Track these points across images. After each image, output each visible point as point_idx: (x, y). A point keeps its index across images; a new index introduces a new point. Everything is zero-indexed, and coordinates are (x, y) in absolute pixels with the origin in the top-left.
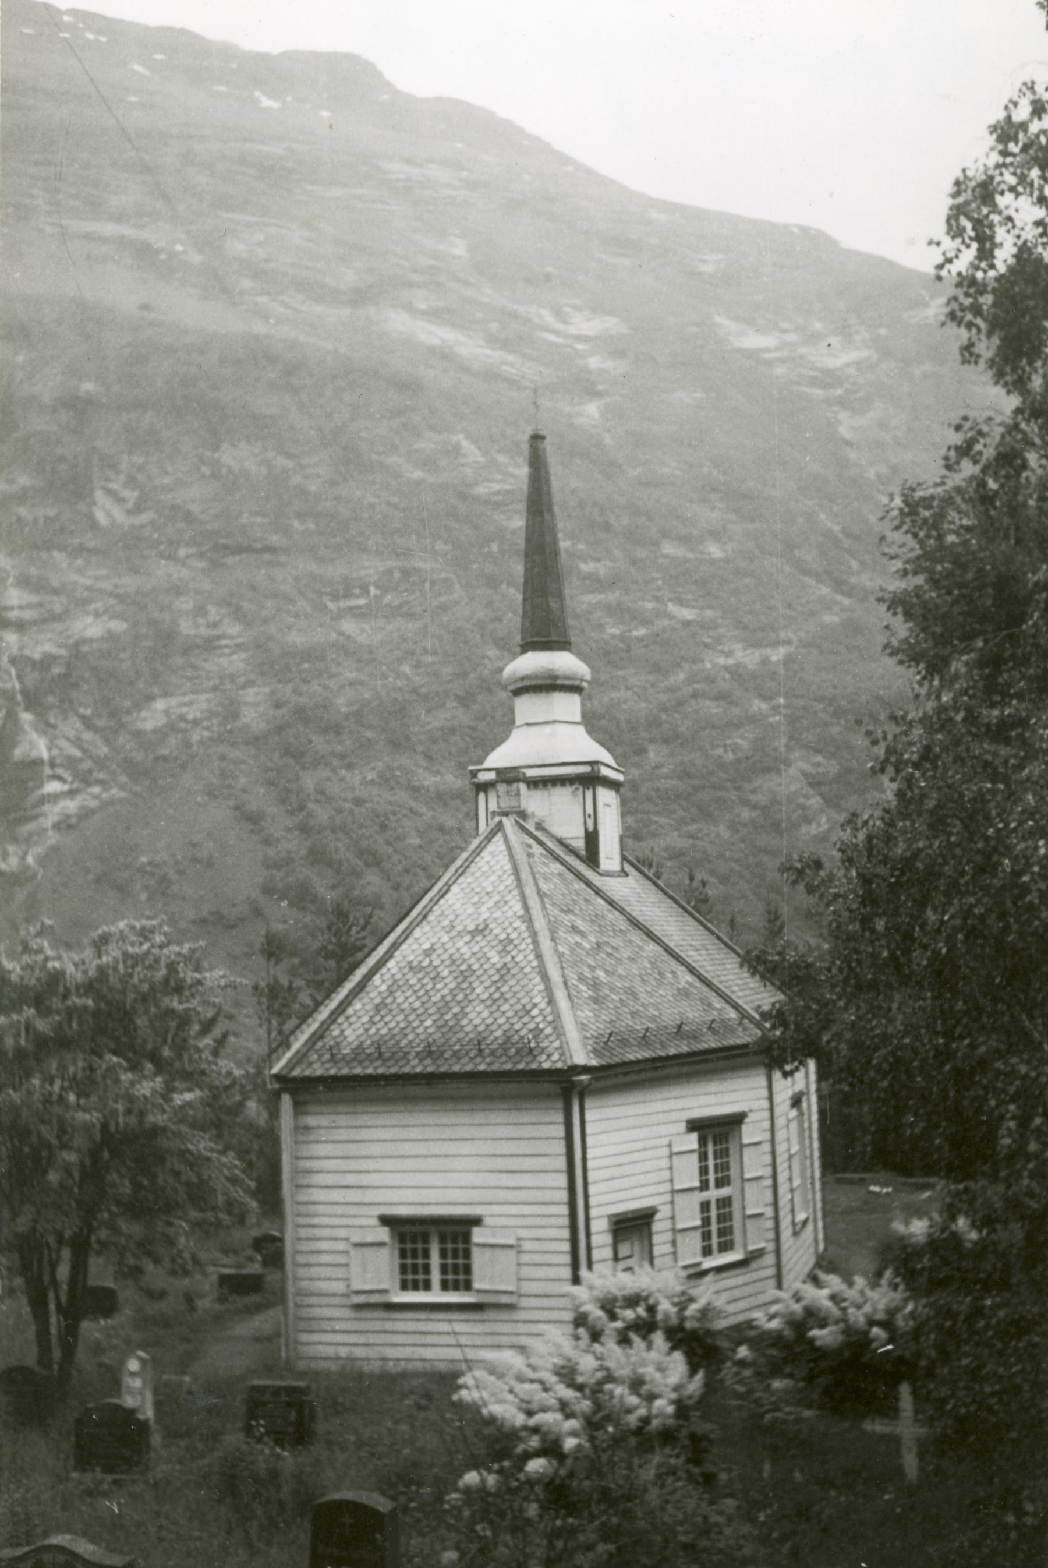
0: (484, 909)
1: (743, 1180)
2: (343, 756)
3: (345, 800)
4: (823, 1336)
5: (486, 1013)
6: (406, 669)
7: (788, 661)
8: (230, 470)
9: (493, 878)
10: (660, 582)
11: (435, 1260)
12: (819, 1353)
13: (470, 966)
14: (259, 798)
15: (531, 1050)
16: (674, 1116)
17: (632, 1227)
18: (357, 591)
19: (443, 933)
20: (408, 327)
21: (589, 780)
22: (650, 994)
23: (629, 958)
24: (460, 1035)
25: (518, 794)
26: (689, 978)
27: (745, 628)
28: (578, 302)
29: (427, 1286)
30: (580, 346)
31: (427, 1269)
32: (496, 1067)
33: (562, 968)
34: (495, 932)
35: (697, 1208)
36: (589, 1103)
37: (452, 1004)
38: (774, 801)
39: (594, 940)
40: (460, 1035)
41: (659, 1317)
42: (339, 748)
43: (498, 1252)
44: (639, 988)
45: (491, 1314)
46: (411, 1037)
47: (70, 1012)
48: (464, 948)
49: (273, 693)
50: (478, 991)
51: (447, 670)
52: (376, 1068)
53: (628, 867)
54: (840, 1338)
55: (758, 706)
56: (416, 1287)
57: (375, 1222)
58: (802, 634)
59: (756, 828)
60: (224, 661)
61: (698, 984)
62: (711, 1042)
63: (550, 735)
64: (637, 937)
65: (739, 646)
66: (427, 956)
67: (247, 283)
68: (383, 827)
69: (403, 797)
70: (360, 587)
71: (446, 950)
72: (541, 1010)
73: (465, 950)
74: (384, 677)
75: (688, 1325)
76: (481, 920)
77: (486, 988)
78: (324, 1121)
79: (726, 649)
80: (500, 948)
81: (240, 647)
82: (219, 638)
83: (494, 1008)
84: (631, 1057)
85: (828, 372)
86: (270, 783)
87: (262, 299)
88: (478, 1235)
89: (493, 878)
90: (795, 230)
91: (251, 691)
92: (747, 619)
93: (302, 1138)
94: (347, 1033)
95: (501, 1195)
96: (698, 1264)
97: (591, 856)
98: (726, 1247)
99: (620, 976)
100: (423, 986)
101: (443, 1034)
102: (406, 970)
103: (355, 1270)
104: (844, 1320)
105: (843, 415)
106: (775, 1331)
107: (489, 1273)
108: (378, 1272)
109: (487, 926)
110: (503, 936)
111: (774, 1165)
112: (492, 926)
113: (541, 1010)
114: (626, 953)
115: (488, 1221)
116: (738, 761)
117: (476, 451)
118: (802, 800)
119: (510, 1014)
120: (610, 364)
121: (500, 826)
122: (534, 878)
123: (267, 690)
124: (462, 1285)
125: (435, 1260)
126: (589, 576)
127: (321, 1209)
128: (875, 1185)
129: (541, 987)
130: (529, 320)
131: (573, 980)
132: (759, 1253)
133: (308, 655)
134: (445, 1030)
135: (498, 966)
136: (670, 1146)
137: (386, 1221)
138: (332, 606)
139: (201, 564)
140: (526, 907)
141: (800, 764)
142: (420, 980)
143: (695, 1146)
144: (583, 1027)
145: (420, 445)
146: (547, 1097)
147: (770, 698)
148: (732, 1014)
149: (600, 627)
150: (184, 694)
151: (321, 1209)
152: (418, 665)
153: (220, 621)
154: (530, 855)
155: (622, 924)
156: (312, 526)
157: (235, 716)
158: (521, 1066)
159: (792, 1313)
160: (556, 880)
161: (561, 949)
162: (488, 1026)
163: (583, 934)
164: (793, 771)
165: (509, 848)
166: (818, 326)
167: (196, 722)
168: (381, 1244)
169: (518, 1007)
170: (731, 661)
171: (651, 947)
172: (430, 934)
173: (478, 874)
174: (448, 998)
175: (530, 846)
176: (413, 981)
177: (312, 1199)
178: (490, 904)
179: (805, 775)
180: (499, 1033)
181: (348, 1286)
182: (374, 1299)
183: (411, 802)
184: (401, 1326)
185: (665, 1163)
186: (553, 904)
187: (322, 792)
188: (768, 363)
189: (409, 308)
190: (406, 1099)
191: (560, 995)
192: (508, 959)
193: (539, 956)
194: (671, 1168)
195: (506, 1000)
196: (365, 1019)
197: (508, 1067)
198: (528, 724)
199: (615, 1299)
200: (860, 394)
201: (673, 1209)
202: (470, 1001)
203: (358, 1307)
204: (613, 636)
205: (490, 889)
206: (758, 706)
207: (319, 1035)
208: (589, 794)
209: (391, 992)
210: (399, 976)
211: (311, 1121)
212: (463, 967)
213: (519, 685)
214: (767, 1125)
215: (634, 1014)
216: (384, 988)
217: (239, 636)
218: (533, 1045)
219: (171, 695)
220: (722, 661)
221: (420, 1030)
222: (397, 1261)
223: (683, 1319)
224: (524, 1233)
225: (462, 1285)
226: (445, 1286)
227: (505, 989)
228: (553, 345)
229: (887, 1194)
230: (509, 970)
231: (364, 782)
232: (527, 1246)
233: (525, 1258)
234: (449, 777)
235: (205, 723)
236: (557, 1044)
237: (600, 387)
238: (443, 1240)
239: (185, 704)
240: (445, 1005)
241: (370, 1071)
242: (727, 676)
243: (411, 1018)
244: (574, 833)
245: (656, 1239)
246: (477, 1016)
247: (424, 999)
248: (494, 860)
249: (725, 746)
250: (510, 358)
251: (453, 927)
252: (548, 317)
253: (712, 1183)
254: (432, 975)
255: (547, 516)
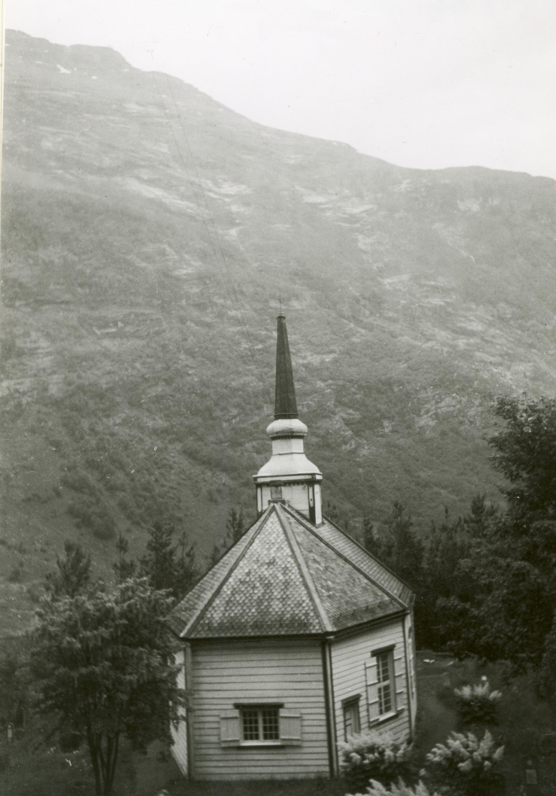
0: (272, 551)
1: (395, 677)
2: (104, 411)
3: (106, 434)
4: (463, 766)
5: (280, 605)
6: (138, 365)
7: (335, 361)
8: (44, 261)
9: (274, 535)
10: (269, 321)
11: (261, 725)
12: (463, 774)
13: (269, 581)
14: (62, 436)
15: (305, 624)
16: (366, 650)
17: (351, 704)
18: (111, 325)
19: (253, 564)
20: (140, 189)
21: (310, 482)
22: (352, 592)
23: (340, 574)
24: (270, 617)
25: (281, 492)
26: (366, 581)
27: (313, 344)
28: (226, 177)
29: (257, 738)
30: (227, 200)
31: (257, 729)
32: (289, 633)
33: (314, 582)
34: (279, 563)
35: (377, 691)
36: (332, 649)
37: (264, 601)
38: (328, 433)
39: (324, 565)
40: (270, 617)
41: (386, 757)
42: (102, 406)
43: (292, 721)
44: (346, 588)
45: (288, 751)
46: (246, 618)
47: (117, 627)
48: (266, 572)
49: (66, 378)
50: (275, 594)
51: (159, 366)
52: (231, 634)
53: (326, 522)
54: (471, 766)
55: (320, 384)
56: (251, 738)
57: (231, 707)
58: (341, 348)
59: (319, 447)
60: (40, 361)
61: (370, 584)
62: (380, 614)
63: (290, 461)
64: (341, 562)
65: (309, 354)
66: (248, 576)
67: (52, 163)
68: (126, 448)
69: (135, 432)
70: (113, 322)
71: (256, 573)
72: (307, 604)
73: (266, 573)
74: (127, 369)
75: (399, 760)
76: (271, 557)
77: (279, 592)
78: (206, 659)
79: (303, 355)
80: (282, 572)
81: (48, 354)
82: (37, 349)
83: (284, 603)
84: (349, 625)
85: (351, 215)
86: (65, 425)
87: (60, 172)
88: (283, 713)
89: (274, 535)
90: (335, 144)
91: (55, 377)
92: (314, 340)
93: (197, 667)
94: (215, 615)
95: (293, 693)
96: (378, 720)
97: (312, 519)
98: (388, 709)
99: (338, 583)
100: (248, 591)
101: (262, 616)
102: (238, 583)
103: (223, 729)
104: (471, 757)
105: (360, 237)
106: (437, 762)
107: (287, 731)
108: (233, 731)
109: (275, 560)
110: (283, 566)
111: (406, 668)
112: (277, 560)
113: (307, 604)
114: (338, 571)
115: (286, 706)
116: (309, 412)
117: (174, 253)
118: (342, 433)
119: (292, 606)
120: (242, 209)
121: (274, 509)
122: (295, 536)
123: (63, 376)
124: (274, 736)
125: (261, 725)
126: (232, 318)
127: (206, 701)
128: (426, 658)
129: (305, 592)
130: (200, 186)
131: (319, 588)
132: (402, 711)
133: (85, 358)
134: (262, 614)
135: (283, 581)
136: (365, 664)
137: (237, 706)
138: (98, 332)
139: (29, 310)
140: (292, 551)
141: (342, 414)
142: (246, 588)
143: (375, 663)
144: (328, 612)
145: (144, 249)
146: (314, 646)
147: (326, 381)
148: (387, 598)
149: (239, 344)
150: (18, 379)
151: (206, 701)
152: (143, 363)
153: (38, 339)
154: (290, 523)
155: (334, 556)
156: (88, 291)
157: (46, 389)
158: (302, 632)
159: (447, 755)
160: (303, 535)
161: (312, 572)
162: (283, 612)
163: (318, 563)
164: (337, 417)
165: (280, 520)
166: (347, 192)
167: (24, 393)
168: (236, 718)
169: (295, 602)
170: (305, 362)
171: (348, 566)
172: (248, 565)
173: (267, 533)
174: (261, 598)
175: (288, 518)
176: (243, 589)
177: (200, 696)
178: (275, 549)
179: (344, 419)
180: (288, 616)
181: (219, 739)
182: (232, 744)
183: (140, 435)
184: (244, 757)
185: (363, 672)
186: (304, 549)
187: (92, 430)
188: (323, 210)
189: (138, 178)
190: (247, 648)
191: (315, 596)
192: (287, 577)
193: (302, 576)
194: (366, 675)
195: (289, 598)
196: (222, 609)
197: (295, 633)
198: (280, 454)
199: (363, 749)
200: (369, 227)
201: (367, 694)
202: (272, 599)
203: (224, 749)
204: (245, 349)
205: (273, 541)
206: (320, 384)
207: (202, 616)
208: (311, 489)
209: (233, 595)
210: (235, 586)
211: (199, 659)
212: (266, 582)
213: (275, 435)
214: (403, 649)
215: (347, 602)
216: (229, 592)
217: (48, 347)
218: (306, 621)
219: (12, 379)
220: (301, 361)
221: (250, 614)
222: (242, 726)
223: (395, 757)
224: (304, 711)
225: (274, 736)
226: (266, 737)
227: (288, 593)
228: (213, 199)
229: (433, 663)
230: (289, 583)
231: (115, 425)
232: (305, 717)
233: (306, 723)
234: (160, 422)
235: (29, 394)
236: (317, 621)
237: (237, 221)
238: (264, 714)
239: (18, 384)
240: (260, 602)
241: (228, 635)
242: (304, 369)
243: (245, 608)
244: (304, 508)
245: (361, 709)
246: (276, 606)
247: (250, 598)
248: (272, 525)
249: (303, 405)
250: (192, 205)
251: (258, 561)
252: (210, 184)
253: (381, 679)
254: (252, 586)
255: (287, 355)
